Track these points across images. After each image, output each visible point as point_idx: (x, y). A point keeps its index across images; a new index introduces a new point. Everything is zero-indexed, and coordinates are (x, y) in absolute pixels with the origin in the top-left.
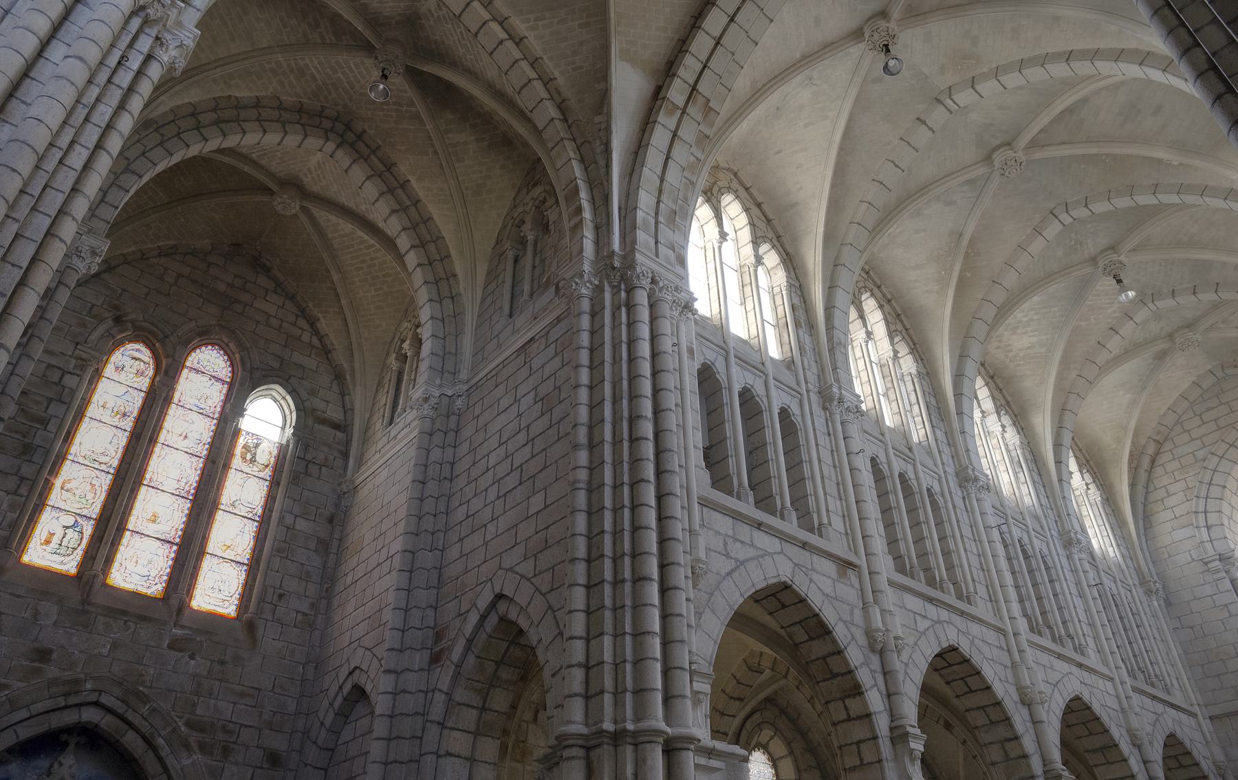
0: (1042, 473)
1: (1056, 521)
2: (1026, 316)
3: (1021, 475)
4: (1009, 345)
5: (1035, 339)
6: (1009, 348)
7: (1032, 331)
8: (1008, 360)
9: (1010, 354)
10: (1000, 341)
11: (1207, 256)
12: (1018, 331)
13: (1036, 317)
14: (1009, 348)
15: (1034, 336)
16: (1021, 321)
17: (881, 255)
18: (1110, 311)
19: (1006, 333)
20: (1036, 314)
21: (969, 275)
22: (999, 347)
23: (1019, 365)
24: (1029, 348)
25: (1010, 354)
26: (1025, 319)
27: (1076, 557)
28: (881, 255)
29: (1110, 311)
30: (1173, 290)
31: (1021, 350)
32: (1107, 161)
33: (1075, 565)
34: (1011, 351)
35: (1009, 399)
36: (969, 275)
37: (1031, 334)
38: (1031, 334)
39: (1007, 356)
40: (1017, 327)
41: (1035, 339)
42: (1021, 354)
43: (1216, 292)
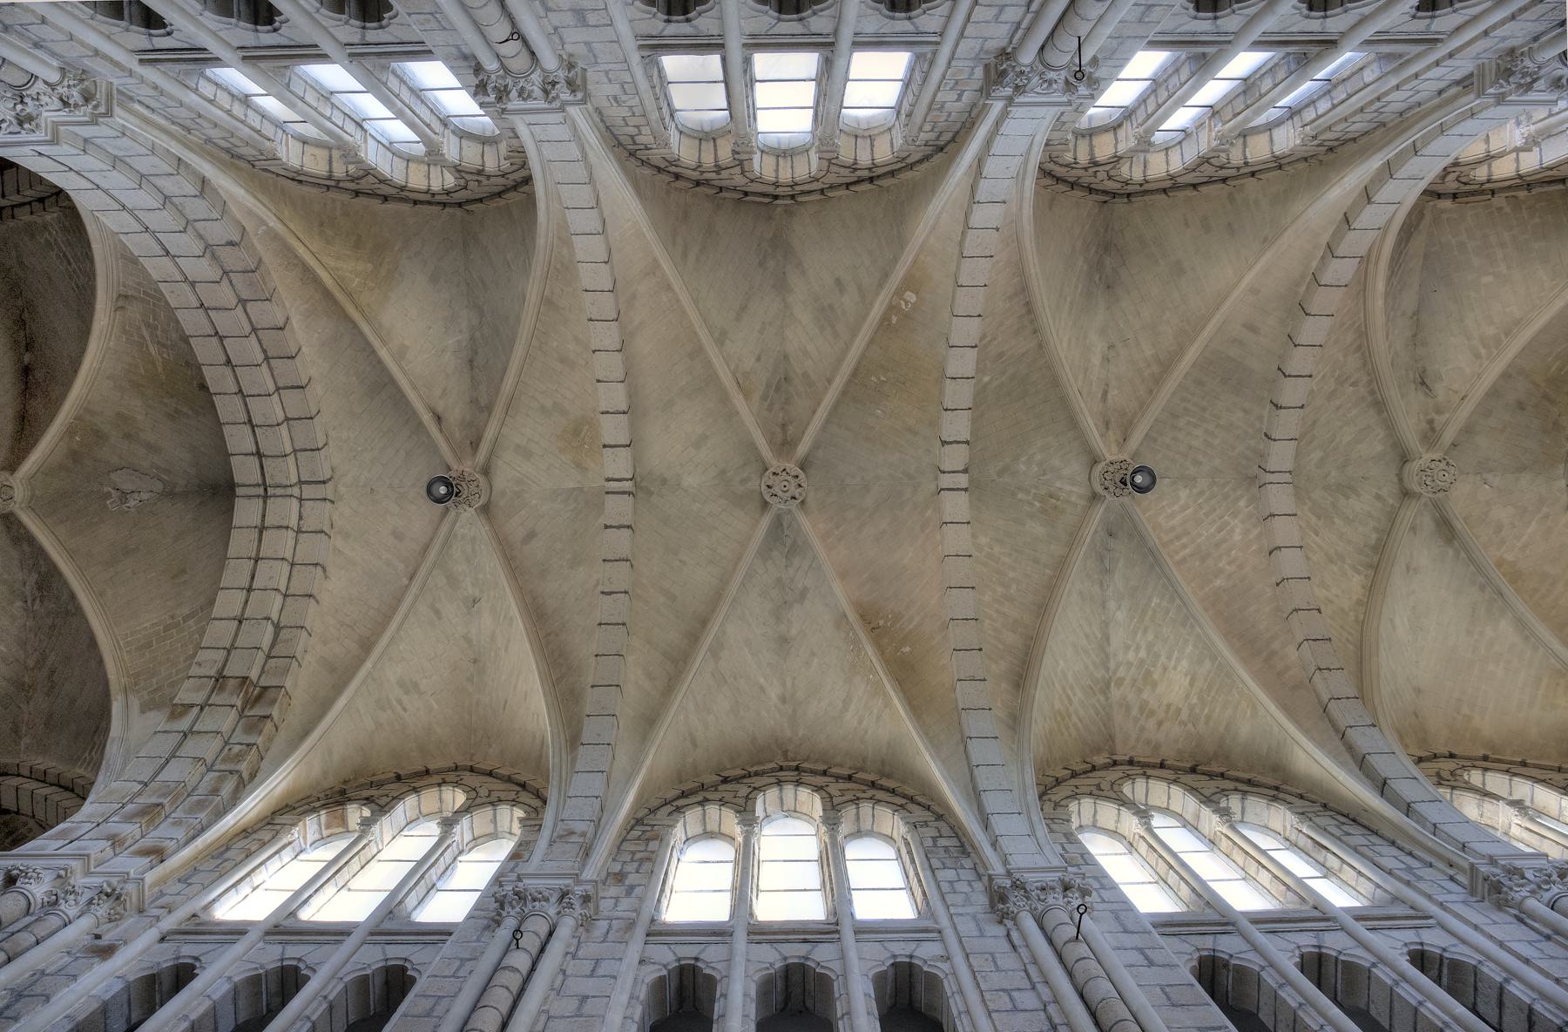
0: (1375, 828)
1: (1452, 879)
2: (1138, 648)
3: (1333, 862)
4: (1169, 706)
5: (1184, 663)
6: (1173, 708)
7: (1169, 658)
8: (1190, 726)
9: (1184, 715)
10: (1152, 713)
11: (1192, 354)
12: (1156, 676)
13: (1150, 637)
14: (1173, 708)
15: (1178, 660)
16: (1142, 661)
17: (801, 733)
18: (1237, 537)
19: (1145, 696)
20: (1145, 631)
21: (907, 649)
22: (1160, 724)
23: (1208, 718)
24: (1191, 684)
25: (1184, 715)
26: (1142, 654)
27: (1532, 903)
28: (801, 733)
29: (1237, 537)
30: (1266, 435)
31: (1187, 697)
32: (883, 378)
33: (1546, 923)
34: (1179, 711)
35: (1247, 776)
36: (907, 649)
37: (1173, 663)
38: (1173, 663)
39: (1183, 723)
40: (1148, 673)
41: (1184, 663)
42: (1195, 701)
43: (1285, 376)
